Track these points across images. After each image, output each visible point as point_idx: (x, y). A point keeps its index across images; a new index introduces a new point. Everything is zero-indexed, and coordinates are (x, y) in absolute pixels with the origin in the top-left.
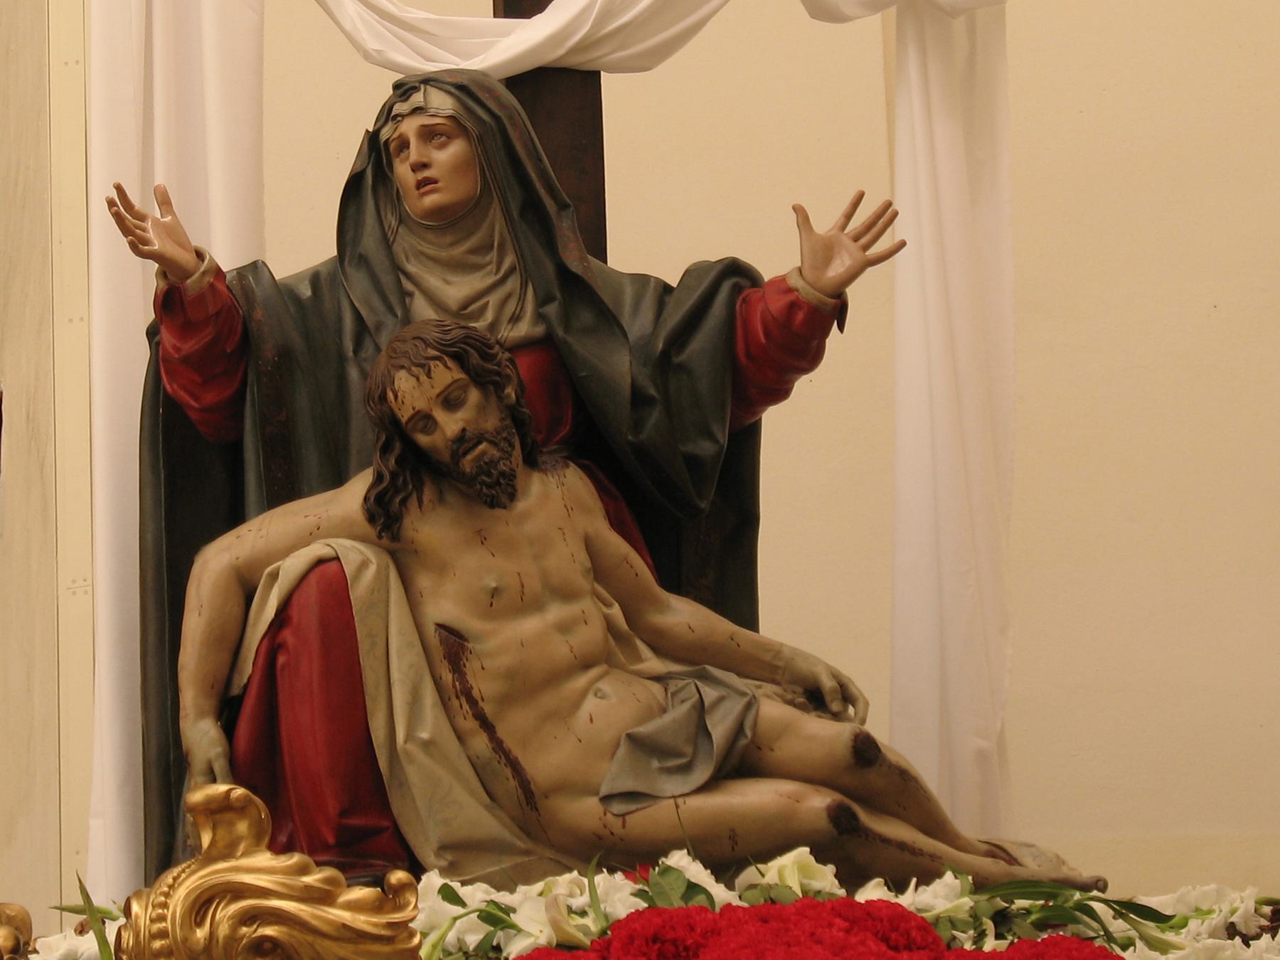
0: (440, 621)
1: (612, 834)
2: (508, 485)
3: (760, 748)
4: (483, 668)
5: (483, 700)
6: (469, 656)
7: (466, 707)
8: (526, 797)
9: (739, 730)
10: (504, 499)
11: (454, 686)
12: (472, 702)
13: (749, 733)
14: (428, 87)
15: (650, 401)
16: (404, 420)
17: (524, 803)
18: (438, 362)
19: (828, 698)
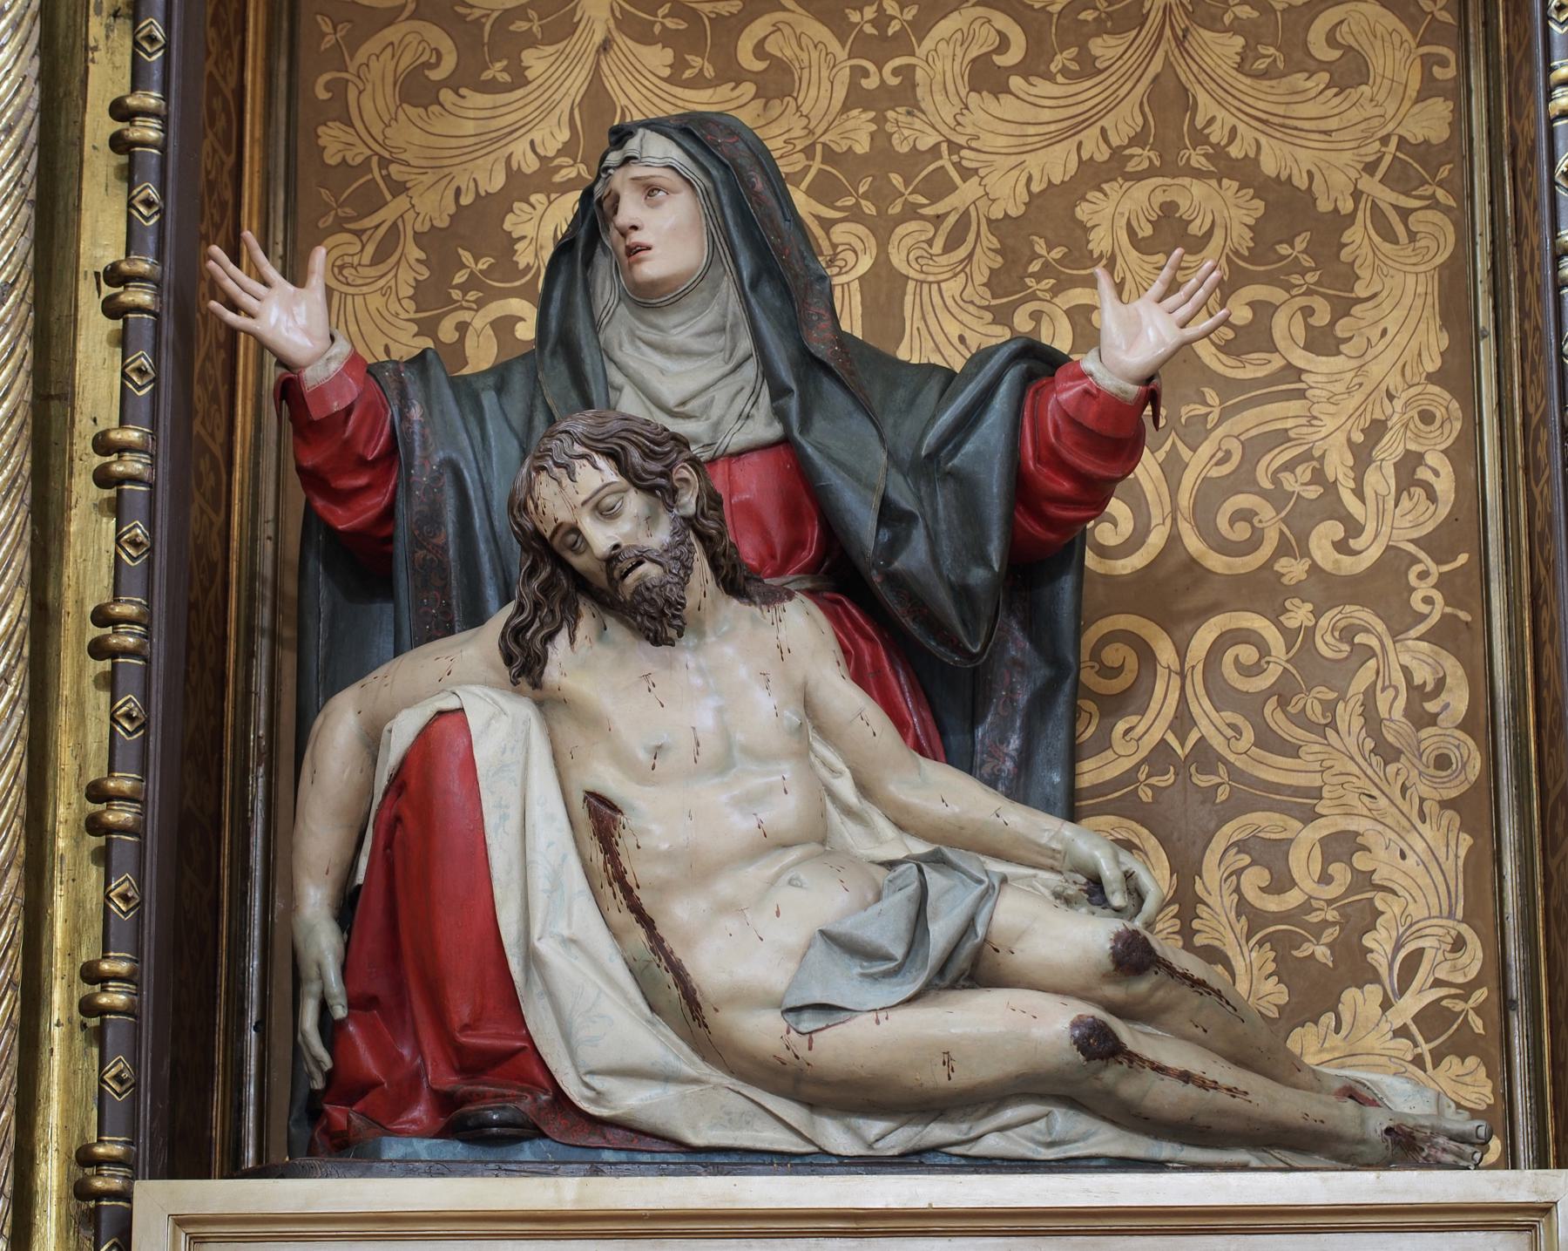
1: (797, 1057)
2: (674, 616)
7: (620, 896)
9: (970, 925)
11: (606, 870)
12: (627, 891)
13: (980, 930)
14: (648, 132)
15: (908, 518)
16: (548, 535)
17: (690, 1018)
18: (585, 462)
19: (1108, 890)
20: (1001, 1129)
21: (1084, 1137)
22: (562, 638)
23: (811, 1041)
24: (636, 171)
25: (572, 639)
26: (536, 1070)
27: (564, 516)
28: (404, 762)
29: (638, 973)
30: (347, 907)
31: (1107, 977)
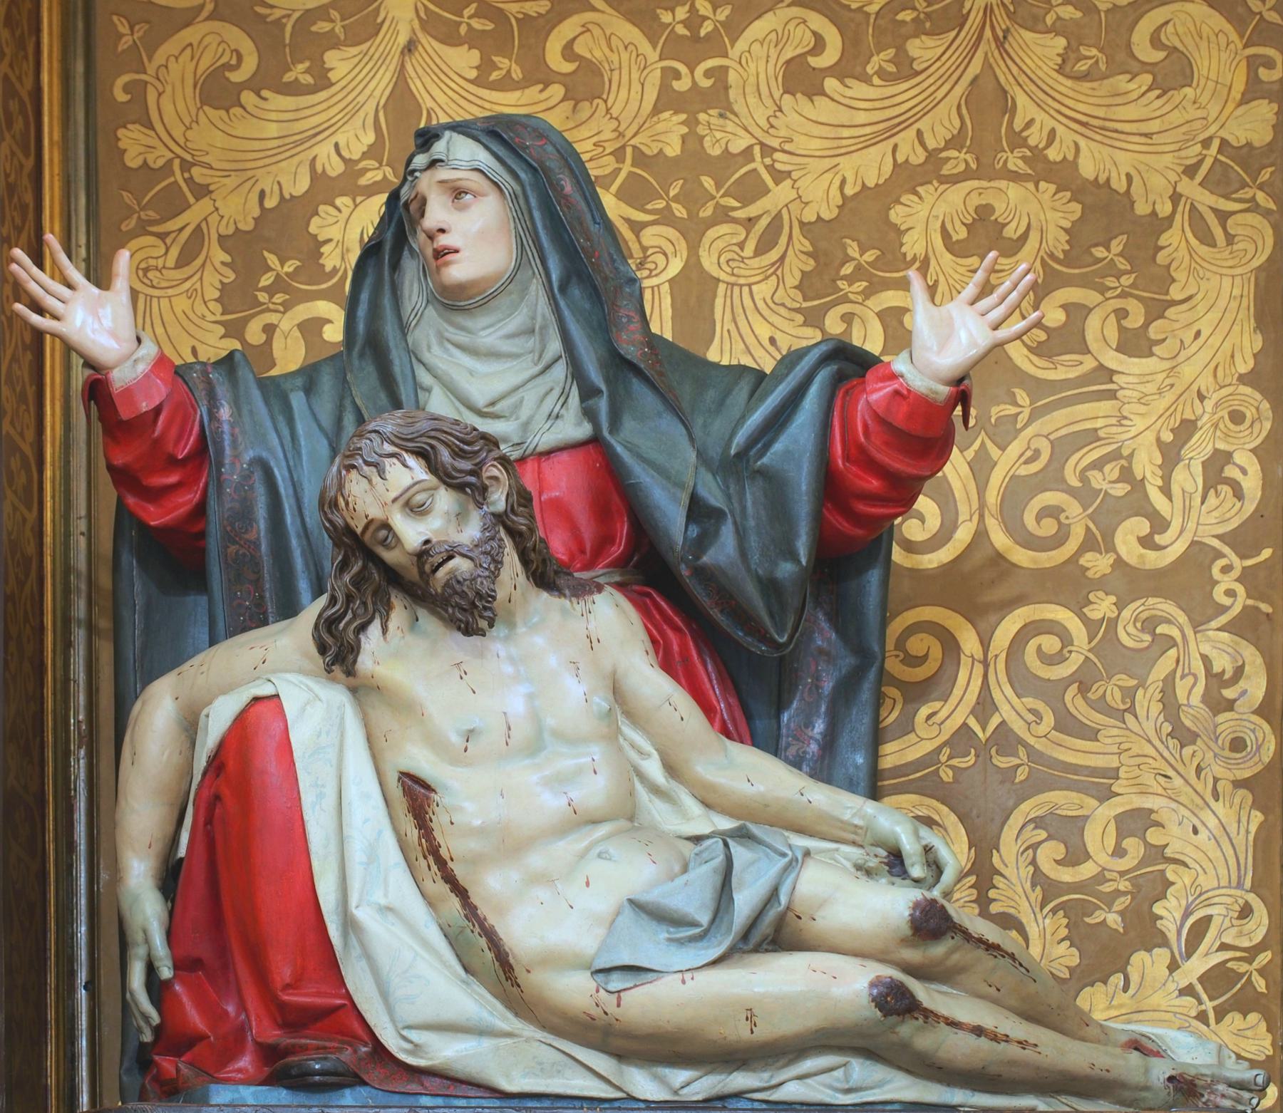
0: (405, 769)
1: (606, 1013)
2: (485, 608)
3: (799, 918)
4: (452, 823)
5: (452, 860)
6: (436, 809)
7: (434, 868)
8: (504, 971)
10: (483, 624)
11: (420, 844)
13: (783, 899)
15: (718, 515)
16: (359, 531)
17: (503, 978)
18: (395, 460)
19: (907, 862)
20: (800, 1078)
22: (375, 629)
23: (619, 999)
24: (443, 174)
25: (385, 630)
27: (375, 512)
28: (222, 745)
31: (904, 942)
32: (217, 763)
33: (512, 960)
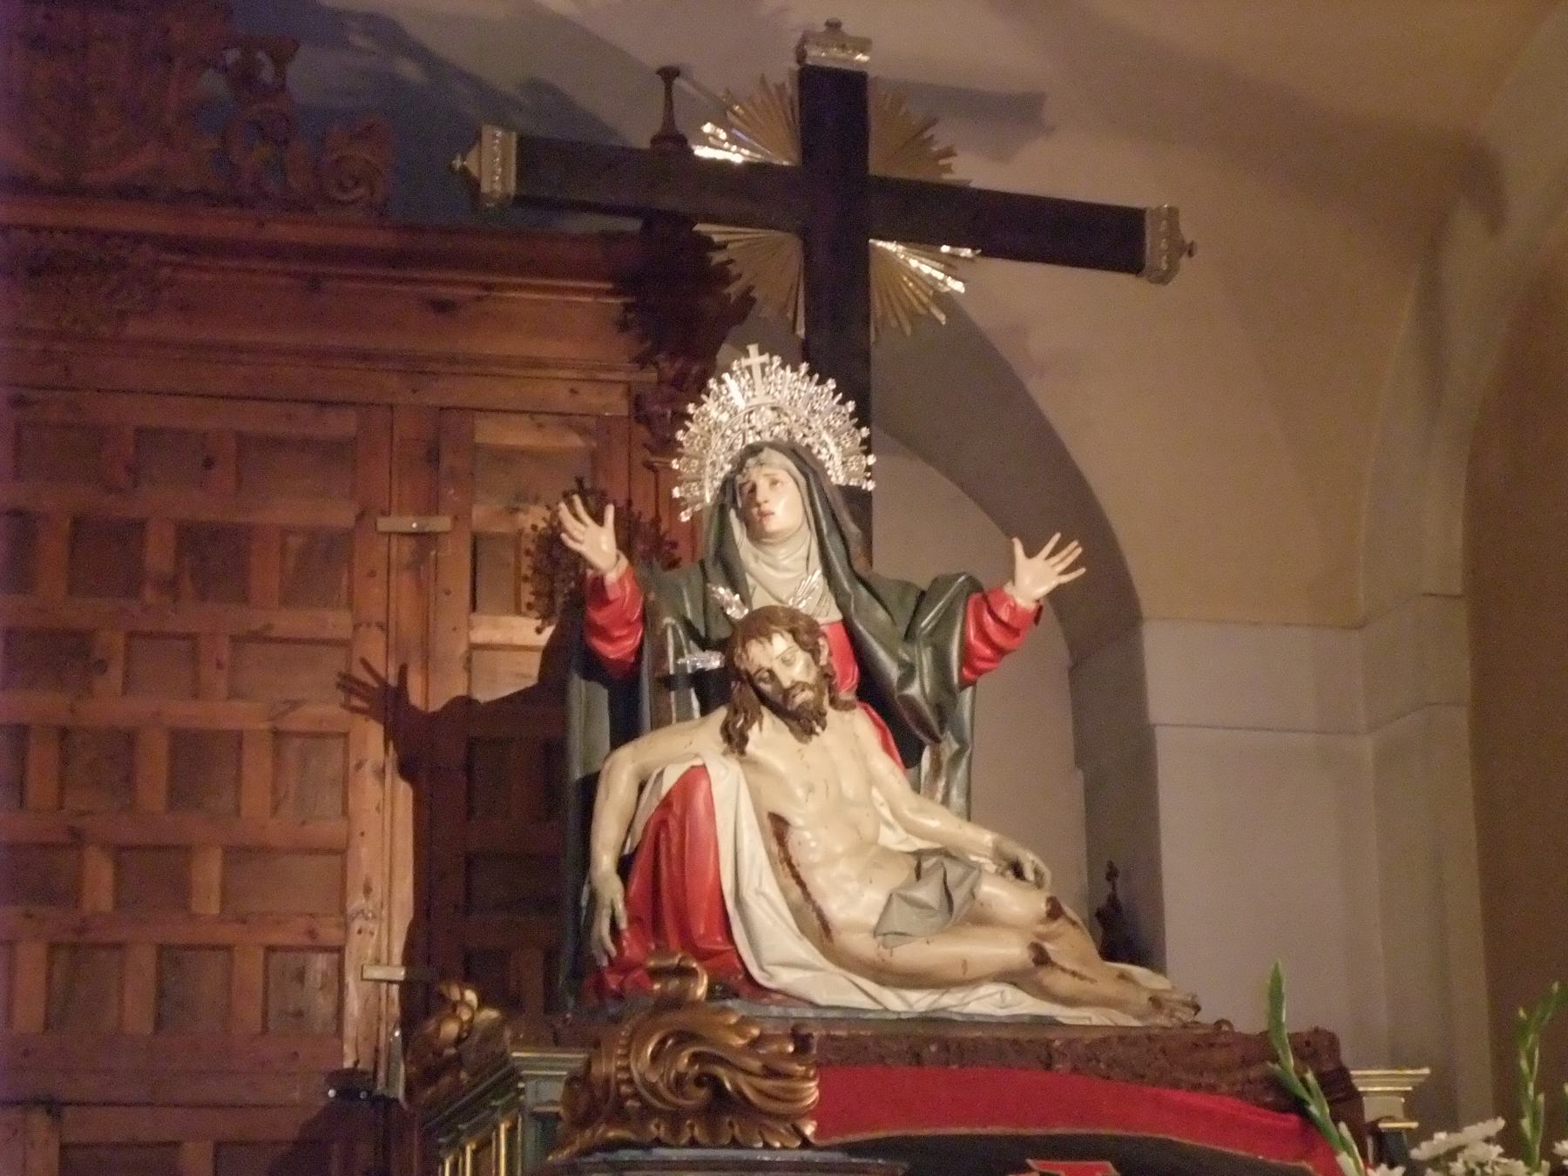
11: (779, 854)
20: (978, 999)
21: (1019, 1004)
22: (756, 727)
23: (892, 952)
24: (766, 470)
25: (761, 729)
26: (736, 961)
27: (766, 664)
28: (669, 793)
29: (795, 911)
30: (624, 866)
31: (1042, 922)
32: (666, 803)
33: (830, 927)
